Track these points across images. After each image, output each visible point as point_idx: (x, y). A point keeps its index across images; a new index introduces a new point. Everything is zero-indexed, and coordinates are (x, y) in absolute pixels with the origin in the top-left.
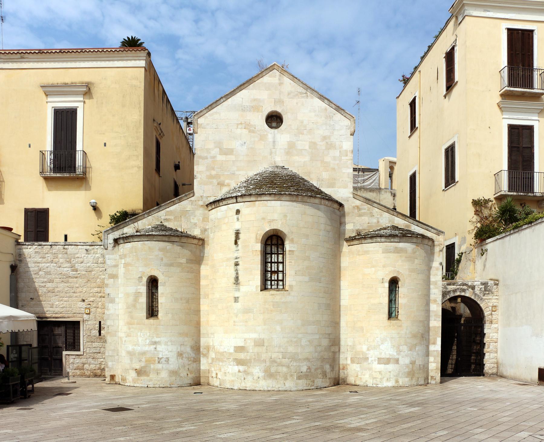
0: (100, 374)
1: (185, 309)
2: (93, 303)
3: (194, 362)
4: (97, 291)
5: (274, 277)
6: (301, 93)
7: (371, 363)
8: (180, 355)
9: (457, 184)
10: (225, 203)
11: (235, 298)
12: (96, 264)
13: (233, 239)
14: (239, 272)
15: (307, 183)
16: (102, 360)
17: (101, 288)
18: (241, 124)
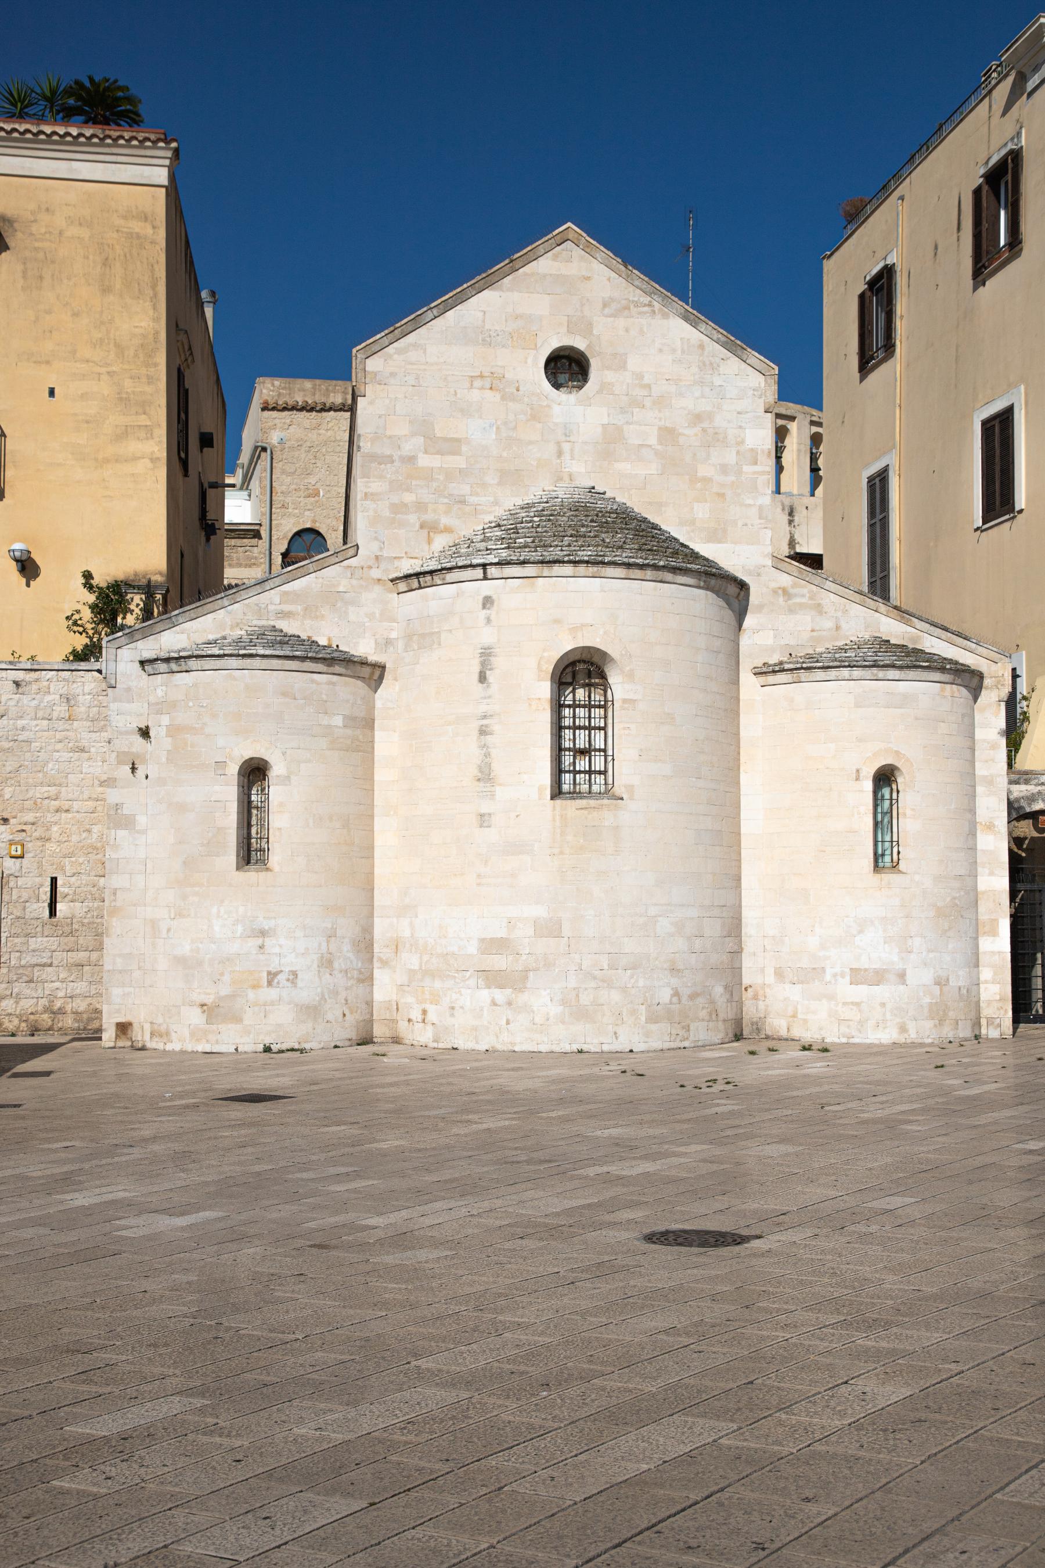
0: (50, 1023)
1: (339, 843)
2: (34, 827)
3: (360, 981)
4: (46, 795)
5: (582, 764)
6: (637, 304)
7: (833, 982)
8: (327, 963)
9: (1020, 516)
10: (450, 577)
11: (482, 815)
12: (46, 722)
13: (476, 669)
14: (494, 752)
15: (659, 532)
16: (57, 984)
17: (60, 785)
18: (481, 376)
